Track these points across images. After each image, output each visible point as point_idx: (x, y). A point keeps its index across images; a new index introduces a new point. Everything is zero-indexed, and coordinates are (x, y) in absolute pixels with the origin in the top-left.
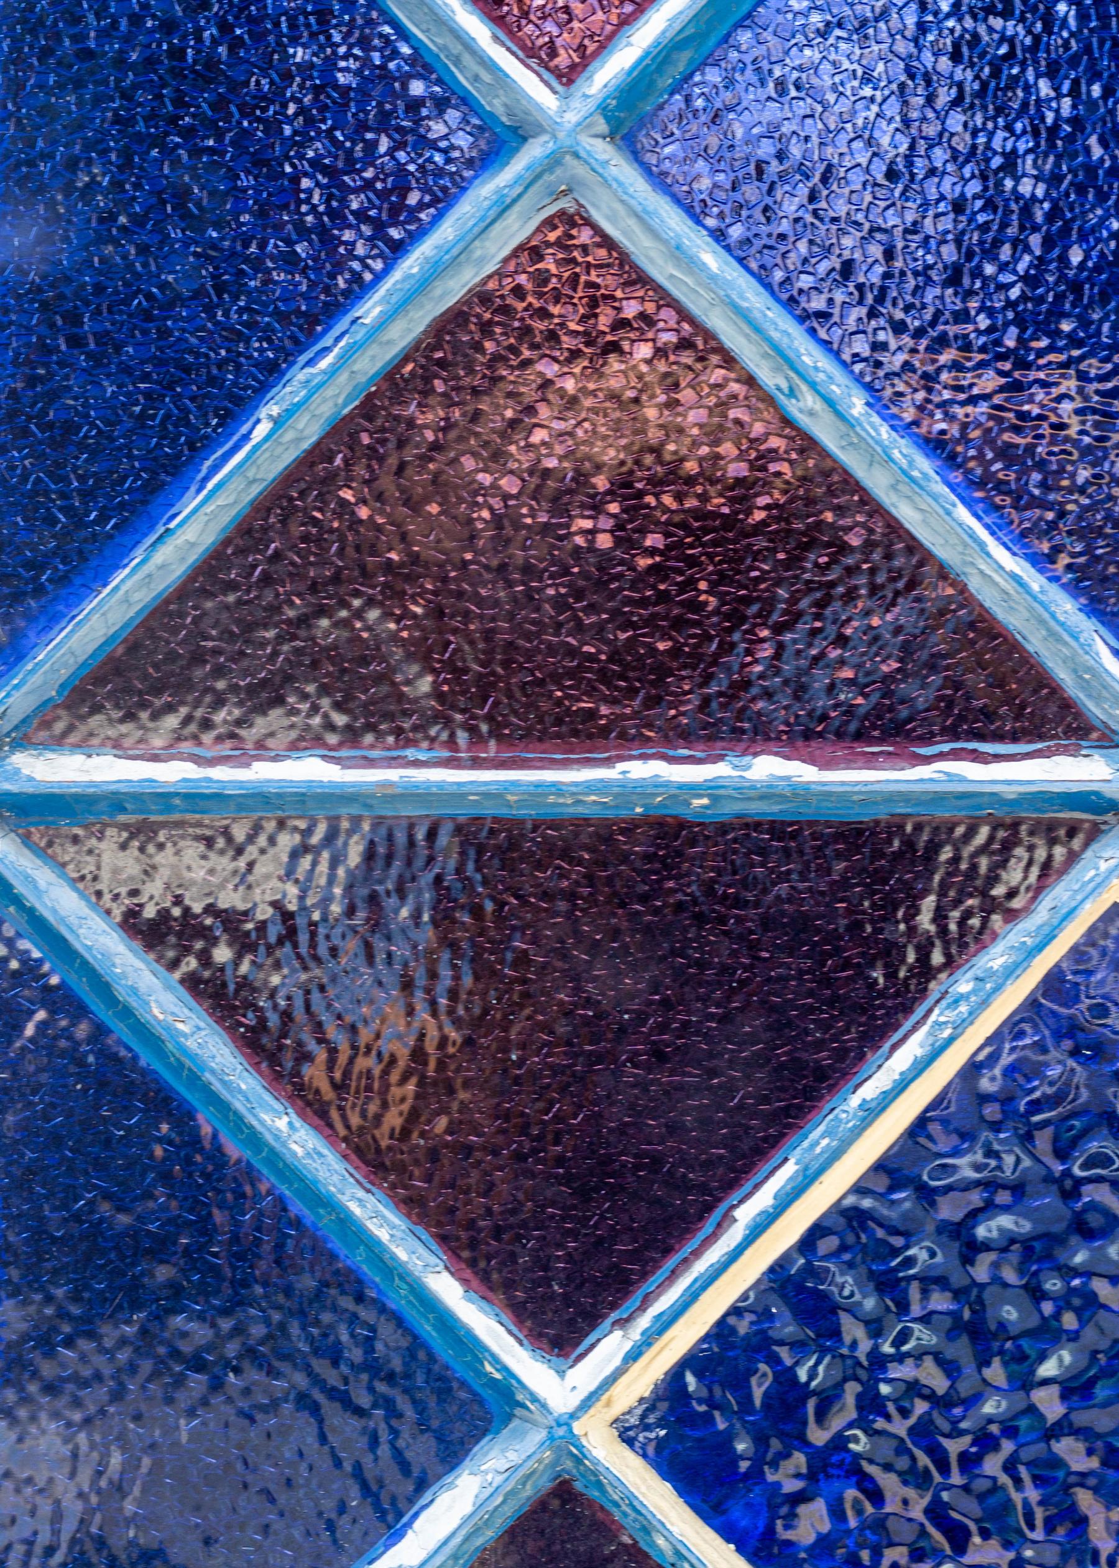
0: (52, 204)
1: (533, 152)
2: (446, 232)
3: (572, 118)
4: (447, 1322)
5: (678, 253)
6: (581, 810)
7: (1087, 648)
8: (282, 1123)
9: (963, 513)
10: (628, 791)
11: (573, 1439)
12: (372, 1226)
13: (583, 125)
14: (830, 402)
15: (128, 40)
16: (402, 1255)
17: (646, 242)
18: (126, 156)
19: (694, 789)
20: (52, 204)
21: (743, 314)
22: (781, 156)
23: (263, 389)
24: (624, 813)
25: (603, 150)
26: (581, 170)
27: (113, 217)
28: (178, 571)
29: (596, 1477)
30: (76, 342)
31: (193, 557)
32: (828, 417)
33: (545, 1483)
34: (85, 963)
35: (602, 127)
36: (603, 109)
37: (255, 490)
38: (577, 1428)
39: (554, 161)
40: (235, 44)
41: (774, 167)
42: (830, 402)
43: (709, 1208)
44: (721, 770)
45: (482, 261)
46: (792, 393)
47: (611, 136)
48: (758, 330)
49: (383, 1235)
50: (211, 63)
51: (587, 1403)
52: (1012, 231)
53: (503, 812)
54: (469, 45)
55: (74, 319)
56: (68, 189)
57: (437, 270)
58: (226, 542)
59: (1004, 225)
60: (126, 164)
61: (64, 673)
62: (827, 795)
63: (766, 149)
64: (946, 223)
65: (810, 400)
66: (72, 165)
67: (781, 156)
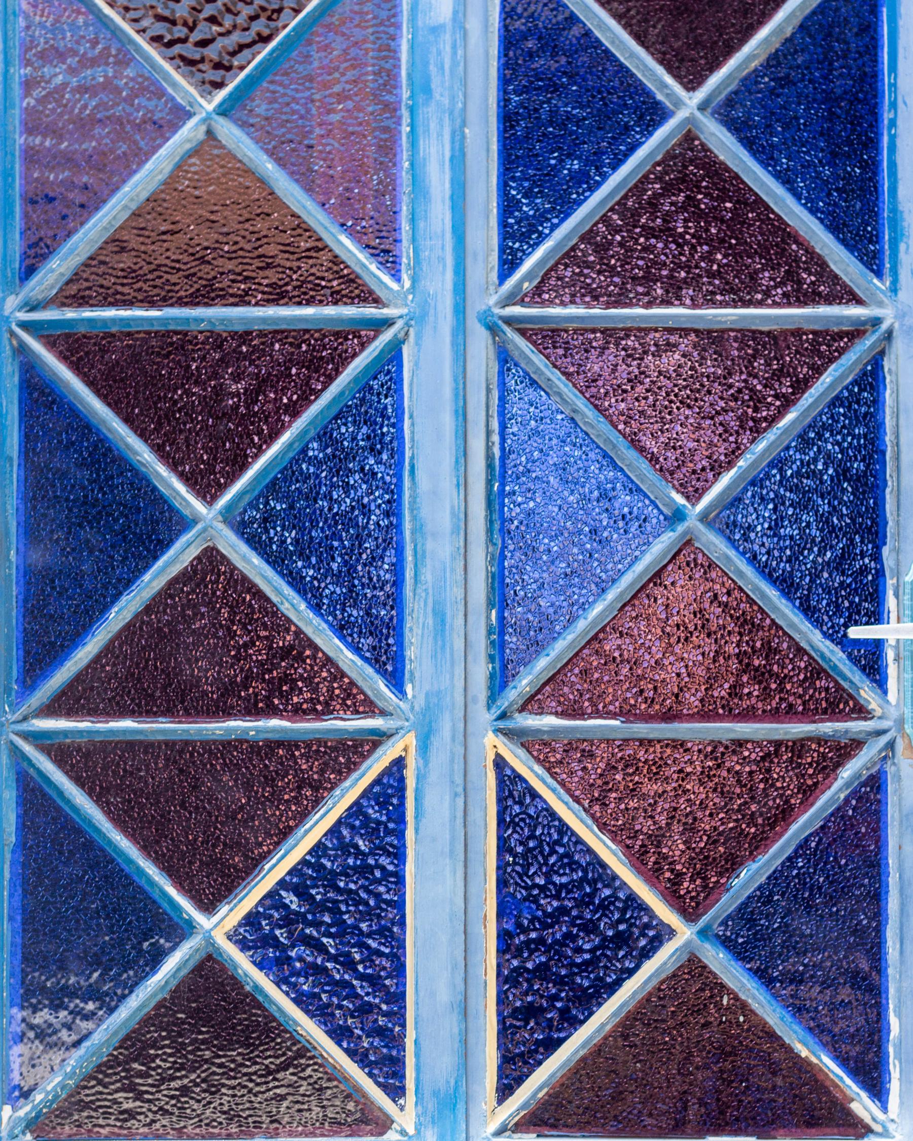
0: (45, 545)
1: (199, 527)
2: (171, 552)
3: (211, 516)
4: (171, 901)
5: (244, 558)
6: (214, 737)
7: (376, 683)
8: (118, 838)
9: (337, 641)
10: (228, 730)
11: (211, 937)
12: (147, 870)
13: (214, 518)
14: (293, 605)
15: (70, 493)
16: (157, 879)
17: (235, 555)
18: (69, 528)
19: (251, 729)
20: (45, 545)
21: (265, 578)
22: (630, 513)
23: (113, 603)
24: (228, 738)
25: (221, 526)
26: (214, 532)
27: (65, 549)
28: (85, 662)
29: (218, 949)
30: (53, 588)
31: (90, 657)
32: (292, 610)
33: (204, 955)
34: (55, 786)
35: (221, 518)
36: (221, 513)
37: (110, 635)
38: (213, 933)
39: (205, 530)
40: (104, 494)
41: (629, 517)
42: (293, 605)
43: (256, 866)
44: (261, 723)
45: (183, 562)
46: (282, 603)
47: (224, 522)
48: (269, 582)
49: (151, 872)
50: (97, 500)
51: (216, 926)
52: (808, 546)
53: (189, 738)
54: (178, 493)
55: (53, 581)
56: (51, 540)
57: (168, 565)
58: (101, 652)
59: (806, 543)
60: (69, 533)
61: (49, 694)
62: (292, 730)
63: (626, 510)
64: (788, 543)
65: (287, 605)
66: (52, 531)
67: (630, 513)
